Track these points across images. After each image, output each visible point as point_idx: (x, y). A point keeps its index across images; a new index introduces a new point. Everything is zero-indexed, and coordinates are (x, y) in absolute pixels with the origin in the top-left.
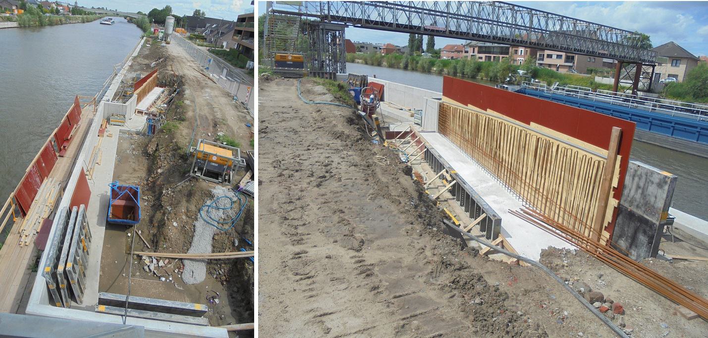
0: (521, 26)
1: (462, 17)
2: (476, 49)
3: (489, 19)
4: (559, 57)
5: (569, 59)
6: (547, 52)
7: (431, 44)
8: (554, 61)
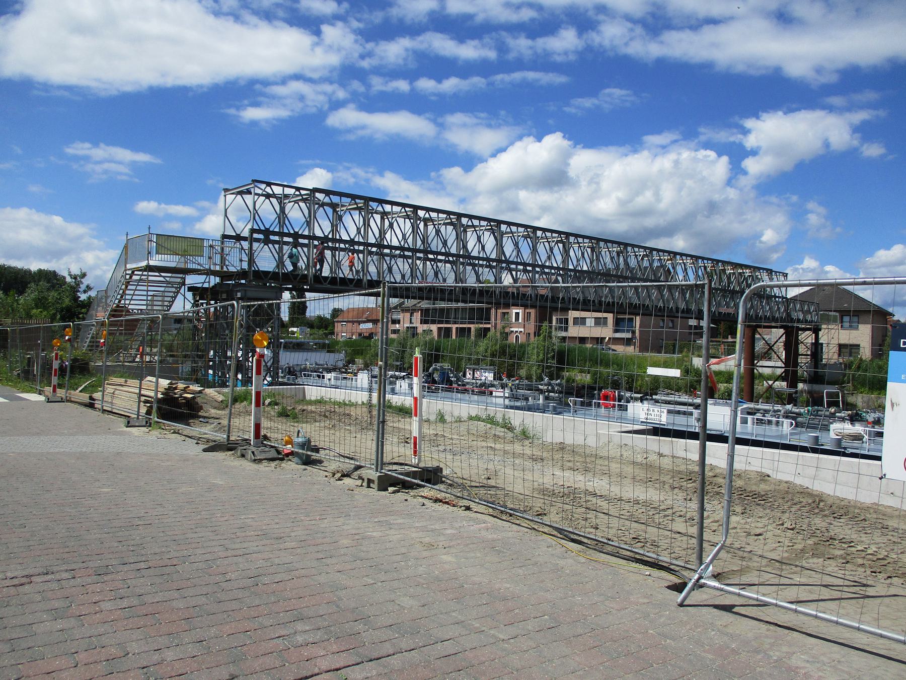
0: (479, 258)
1: (342, 246)
2: (417, 316)
3: (406, 246)
4: (599, 322)
5: (618, 325)
6: (573, 314)
7: (299, 309)
8: (589, 330)
